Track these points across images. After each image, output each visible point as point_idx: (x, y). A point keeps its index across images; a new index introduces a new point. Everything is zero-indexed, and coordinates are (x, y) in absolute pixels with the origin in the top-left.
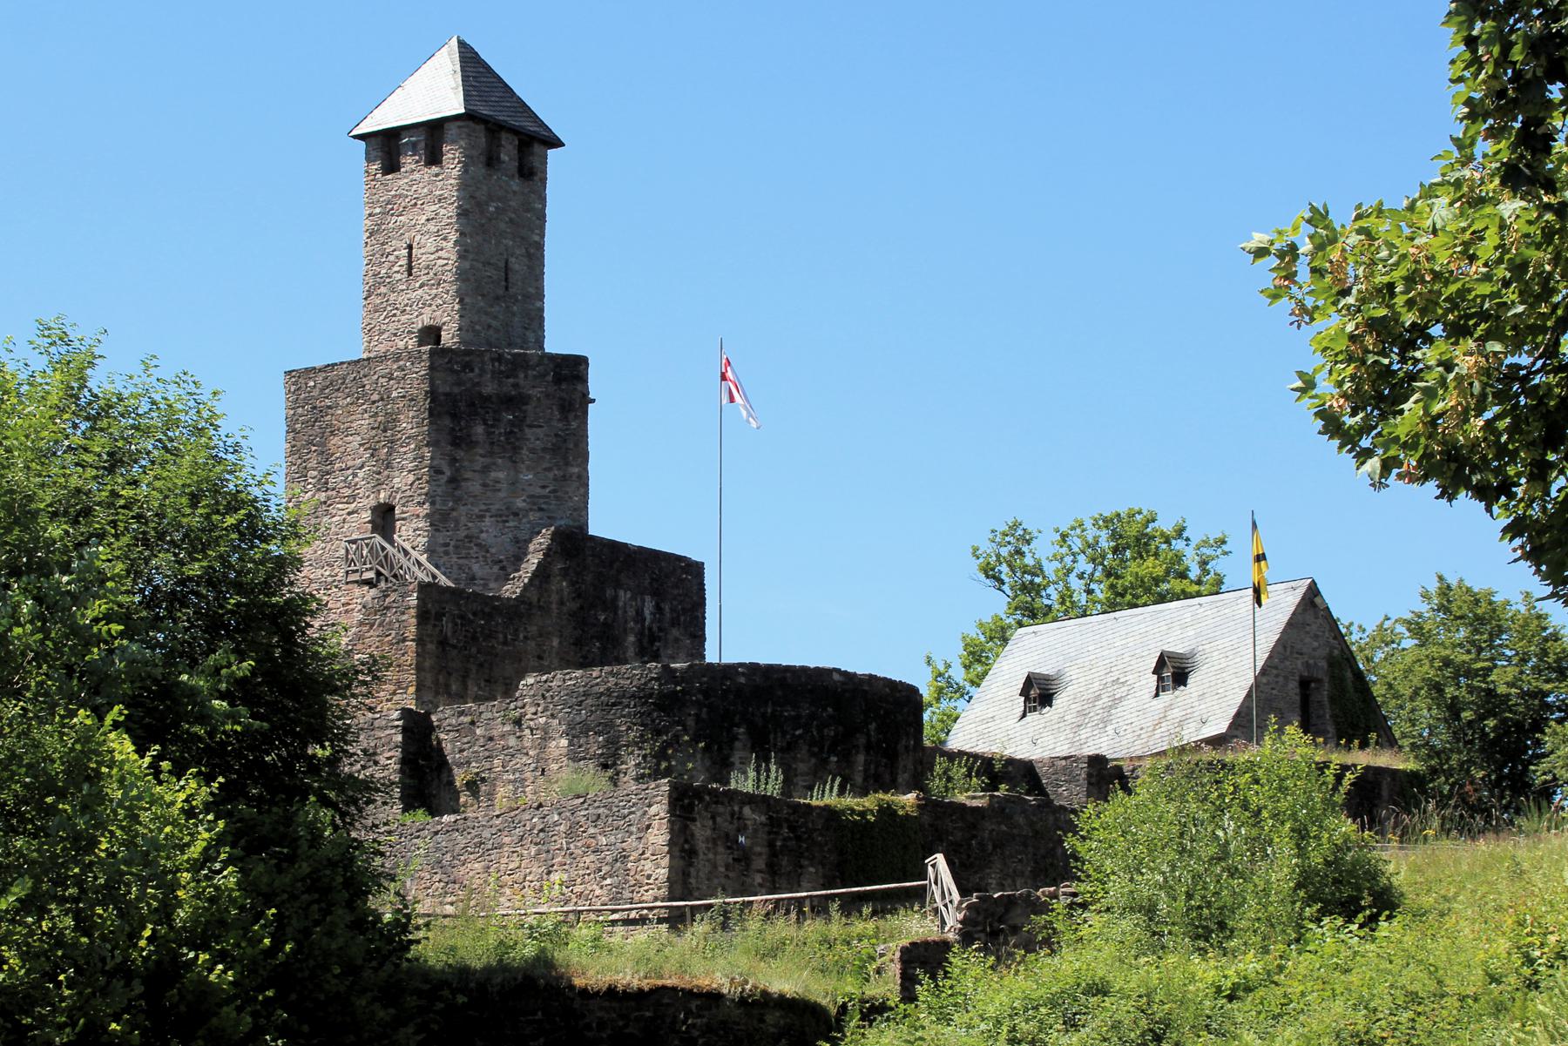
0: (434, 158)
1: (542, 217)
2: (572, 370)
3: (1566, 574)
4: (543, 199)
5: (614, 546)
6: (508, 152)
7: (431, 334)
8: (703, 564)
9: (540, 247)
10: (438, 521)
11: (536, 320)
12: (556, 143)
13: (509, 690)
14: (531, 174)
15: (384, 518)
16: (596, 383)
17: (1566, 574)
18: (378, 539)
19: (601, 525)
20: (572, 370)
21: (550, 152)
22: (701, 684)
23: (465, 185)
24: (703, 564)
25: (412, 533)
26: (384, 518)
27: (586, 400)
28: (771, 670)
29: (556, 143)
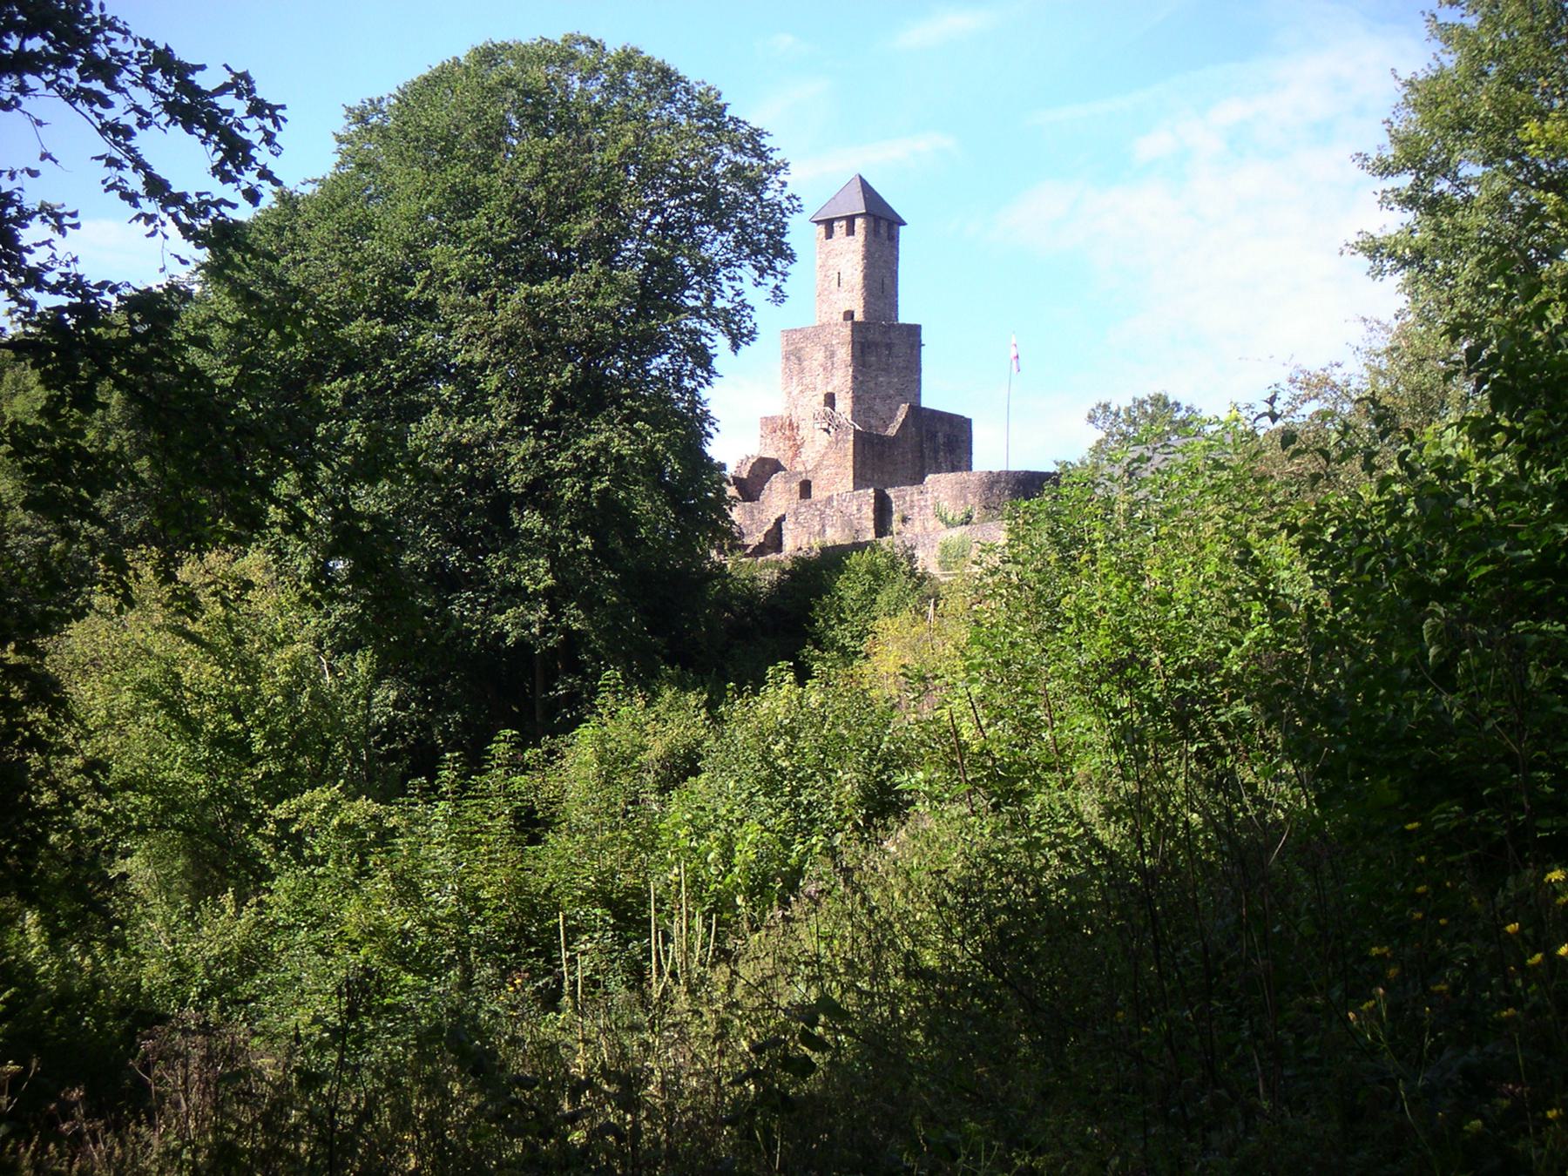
0: (850, 231)
1: (897, 259)
2: (914, 330)
3: (1563, 951)
4: (897, 249)
5: (934, 413)
6: (883, 230)
7: (849, 315)
8: (969, 422)
9: (896, 272)
10: (857, 399)
11: (894, 306)
12: (904, 224)
13: (921, 481)
14: (893, 239)
15: (830, 400)
16: (925, 337)
17: (1563, 951)
18: (828, 409)
19: (926, 402)
20: (914, 330)
21: (901, 228)
22: (473, 469)
23: (868, 245)
24: (969, 422)
25: (844, 405)
26: (830, 400)
27: (920, 345)
28: (1034, 473)
29: (904, 224)
